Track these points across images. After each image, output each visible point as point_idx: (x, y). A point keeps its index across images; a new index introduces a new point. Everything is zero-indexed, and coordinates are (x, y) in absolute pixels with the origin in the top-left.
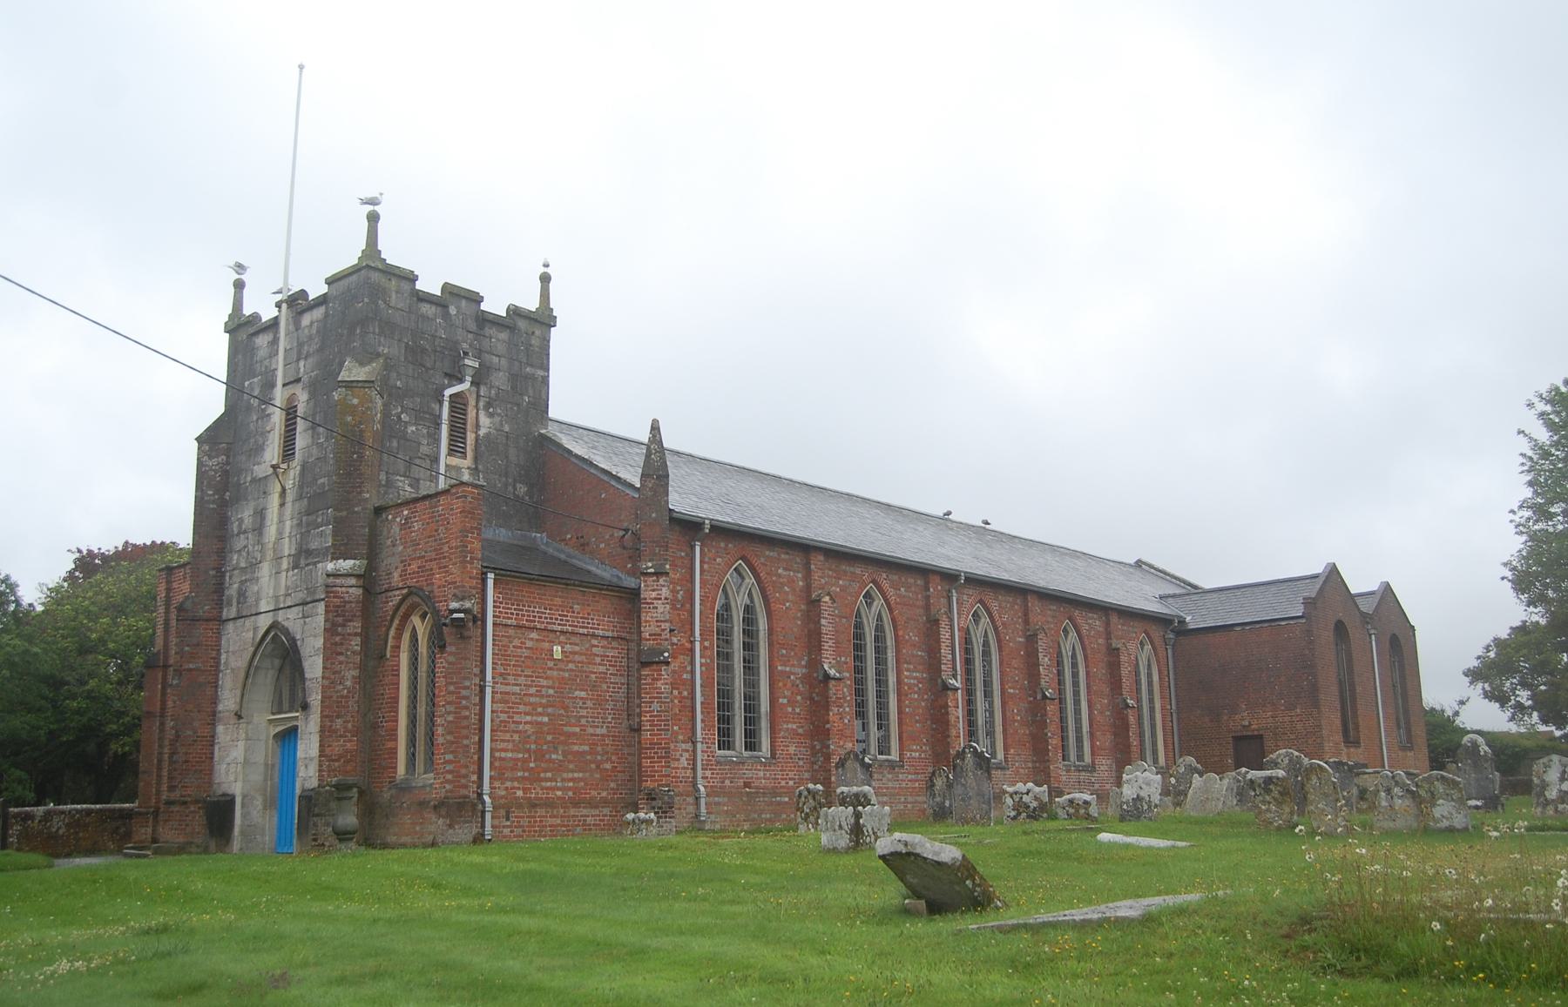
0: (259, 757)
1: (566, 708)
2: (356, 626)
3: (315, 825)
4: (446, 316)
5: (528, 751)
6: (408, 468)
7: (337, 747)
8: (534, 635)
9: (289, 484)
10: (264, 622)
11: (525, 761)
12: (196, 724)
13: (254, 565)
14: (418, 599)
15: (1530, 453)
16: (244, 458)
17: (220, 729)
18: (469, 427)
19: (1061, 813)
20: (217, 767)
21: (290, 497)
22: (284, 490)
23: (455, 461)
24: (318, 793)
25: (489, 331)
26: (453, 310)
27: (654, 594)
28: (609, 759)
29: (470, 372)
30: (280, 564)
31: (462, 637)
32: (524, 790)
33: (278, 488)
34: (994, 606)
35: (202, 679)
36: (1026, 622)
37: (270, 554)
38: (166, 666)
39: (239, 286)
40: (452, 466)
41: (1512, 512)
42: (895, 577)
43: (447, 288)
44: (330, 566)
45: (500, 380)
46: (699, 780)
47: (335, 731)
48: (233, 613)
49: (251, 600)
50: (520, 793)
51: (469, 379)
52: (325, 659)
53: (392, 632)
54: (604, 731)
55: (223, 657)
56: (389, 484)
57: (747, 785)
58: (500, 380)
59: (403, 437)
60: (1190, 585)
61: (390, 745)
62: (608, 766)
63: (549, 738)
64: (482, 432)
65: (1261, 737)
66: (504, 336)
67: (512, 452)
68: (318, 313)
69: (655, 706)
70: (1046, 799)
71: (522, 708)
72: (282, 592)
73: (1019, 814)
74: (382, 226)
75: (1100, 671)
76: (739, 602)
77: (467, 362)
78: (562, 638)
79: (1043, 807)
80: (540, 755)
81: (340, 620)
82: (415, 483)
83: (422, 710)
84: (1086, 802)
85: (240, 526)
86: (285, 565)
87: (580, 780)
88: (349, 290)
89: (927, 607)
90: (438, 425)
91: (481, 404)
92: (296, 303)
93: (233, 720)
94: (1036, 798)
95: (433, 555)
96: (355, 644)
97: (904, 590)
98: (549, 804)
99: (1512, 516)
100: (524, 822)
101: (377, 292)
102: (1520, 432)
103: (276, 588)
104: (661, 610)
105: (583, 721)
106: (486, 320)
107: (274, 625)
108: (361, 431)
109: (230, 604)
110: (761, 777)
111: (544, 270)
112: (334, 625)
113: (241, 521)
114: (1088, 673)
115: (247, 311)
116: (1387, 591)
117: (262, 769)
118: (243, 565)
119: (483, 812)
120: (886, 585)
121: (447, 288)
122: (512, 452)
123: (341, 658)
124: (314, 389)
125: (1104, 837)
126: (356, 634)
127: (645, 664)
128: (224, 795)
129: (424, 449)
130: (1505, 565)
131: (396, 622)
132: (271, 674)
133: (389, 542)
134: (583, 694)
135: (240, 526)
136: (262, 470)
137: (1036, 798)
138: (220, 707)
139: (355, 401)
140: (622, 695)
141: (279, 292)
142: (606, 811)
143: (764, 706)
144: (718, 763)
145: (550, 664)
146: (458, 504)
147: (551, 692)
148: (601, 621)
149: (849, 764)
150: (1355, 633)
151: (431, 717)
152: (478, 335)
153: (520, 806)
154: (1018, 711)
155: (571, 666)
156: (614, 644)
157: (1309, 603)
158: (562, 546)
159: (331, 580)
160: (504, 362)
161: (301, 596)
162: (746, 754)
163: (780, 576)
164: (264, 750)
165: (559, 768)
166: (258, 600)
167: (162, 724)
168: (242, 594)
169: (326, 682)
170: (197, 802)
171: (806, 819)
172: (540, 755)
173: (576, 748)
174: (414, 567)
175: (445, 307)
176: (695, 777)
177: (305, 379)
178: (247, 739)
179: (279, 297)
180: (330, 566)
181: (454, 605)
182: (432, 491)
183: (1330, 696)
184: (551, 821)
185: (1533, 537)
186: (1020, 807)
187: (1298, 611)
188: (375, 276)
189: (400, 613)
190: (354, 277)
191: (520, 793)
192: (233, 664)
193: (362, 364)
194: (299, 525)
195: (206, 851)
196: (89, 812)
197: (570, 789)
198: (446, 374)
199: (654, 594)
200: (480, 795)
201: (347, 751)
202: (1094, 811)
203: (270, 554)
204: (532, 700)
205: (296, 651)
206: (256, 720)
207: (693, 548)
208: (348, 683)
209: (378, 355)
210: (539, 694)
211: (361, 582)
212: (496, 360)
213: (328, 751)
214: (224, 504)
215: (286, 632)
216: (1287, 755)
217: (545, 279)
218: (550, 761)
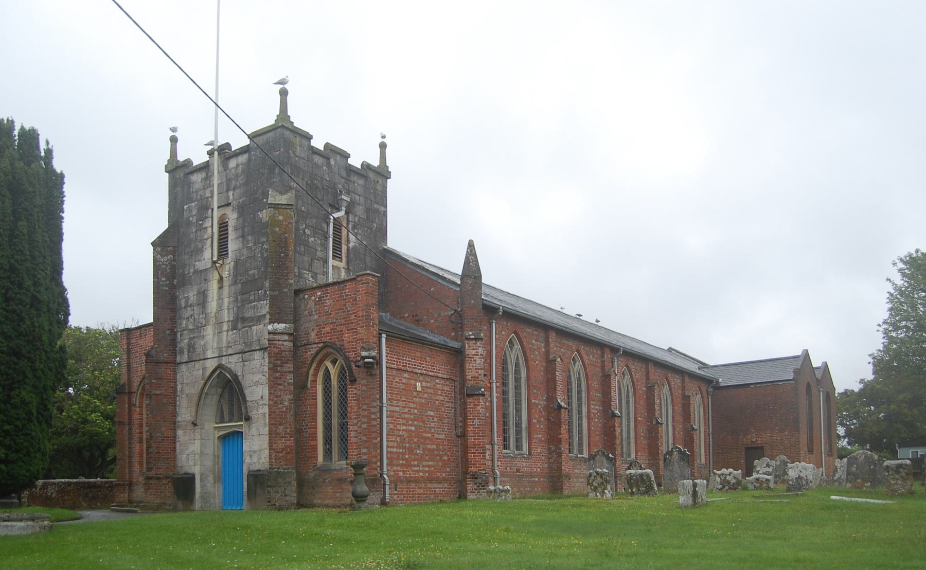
0: (210, 451)
1: (423, 422)
2: (289, 367)
3: (269, 492)
4: (329, 165)
5: (405, 448)
6: (311, 265)
7: (280, 444)
8: (406, 375)
9: (225, 274)
10: (211, 365)
11: (404, 454)
12: (163, 429)
13: (199, 328)
14: (330, 350)
15: (892, 291)
16: (187, 257)
17: (180, 432)
18: (343, 241)
19: (750, 486)
20: (179, 456)
21: (226, 283)
22: (221, 279)
23: (337, 263)
24: (270, 473)
25: (354, 178)
26: (332, 162)
27: (474, 352)
28: (446, 454)
29: (345, 204)
30: (221, 328)
31: (371, 375)
32: (404, 472)
33: (216, 276)
34: (633, 368)
35: (165, 401)
36: (648, 379)
37: (212, 320)
38: (130, 393)
39: (174, 140)
40: (336, 269)
41: (879, 325)
42: (587, 349)
43: (327, 146)
44: (270, 327)
45: (360, 210)
46: (496, 468)
47: (279, 434)
48: (185, 358)
49: (199, 350)
50: (401, 474)
51: (344, 208)
52: (270, 388)
53: (311, 371)
54: (442, 436)
55: (179, 387)
56: (300, 275)
57: (518, 471)
58: (360, 210)
59: (307, 245)
60: (701, 362)
61: (312, 443)
62: (446, 458)
63: (415, 440)
64: (351, 245)
65: (762, 448)
66: (361, 182)
67: (368, 259)
68: (243, 158)
69: (476, 422)
70: (740, 478)
71: (401, 421)
72: (224, 344)
73: (724, 487)
74: (289, 98)
75: (679, 409)
76: (512, 358)
77: (344, 197)
78: (421, 378)
79: (739, 483)
80: (411, 451)
81: (279, 362)
82: (315, 276)
83: (335, 421)
84: (767, 480)
85: (187, 302)
86: (225, 327)
87: (432, 466)
88: (268, 143)
89: (603, 367)
90: (327, 238)
91: (350, 226)
92: (224, 152)
93: (190, 427)
94: (735, 478)
95: (343, 321)
96: (290, 378)
97: (592, 356)
98: (416, 481)
99: (878, 328)
100: (405, 491)
101: (289, 145)
102: (888, 280)
103: (220, 341)
104: (478, 362)
105: (433, 430)
106: (351, 170)
107: (220, 366)
108: (286, 238)
109: (182, 352)
110: (524, 465)
111: (382, 140)
112: (275, 366)
113: (187, 299)
114: (673, 410)
115: (181, 158)
116: (825, 366)
117: (211, 458)
118: (191, 327)
119: (385, 485)
120: (583, 353)
121: (327, 146)
122: (368, 259)
123: (281, 387)
124: (242, 210)
125: (833, 497)
126: (290, 372)
127: (469, 396)
128: (186, 474)
129: (319, 254)
130: (870, 355)
131: (314, 365)
132: (215, 398)
133: (306, 313)
134: (432, 413)
135: (187, 302)
136: (200, 265)
137: (735, 478)
138: (179, 419)
139: (281, 218)
140: (451, 415)
141: (211, 144)
142: (446, 485)
143: (524, 424)
144: (504, 457)
145: (415, 394)
146: (362, 288)
147: (416, 411)
148: (440, 368)
149: (598, 458)
150: (814, 390)
151: (343, 427)
152: (348, 180)
153: (402, 482)
154: (642, 430)
155: (426, 396)
156: (448, 383)
157: (796, 372)
158: (402, 321)
159: (271, 336)
160: (362, 200)
161: (240, 348)
162: (516, 452)
163: (533, 345)
164: (212, 446)
165: (421, 459)
166: (205, 350)
167: (130, 429)
168: (191, 347)
169: (272, 403)
170: (167, 478)
171: (595, 489)
172: (411, 451)
173: (429, 446)
174: (328, 329)
175: (328, 159)
176: (493, 465)
177: (235, 203)
178: (202, 439)
179: (210, 147)
180: (270, 327)
181: (364, 354)
182: (324, 282)
183: (803, 427)
184: (419, 491)
185: (891, 340)
186: (725, 483)
187: (790, 376)
188: (287, 133)
189: (318, 358)
190: (271, 134)
191: (401, 474)
192: (187, 391)
193: (281, 193)
194: (236, 300)
195: (175, 509)
196: (70, 484)
197: (427, 471)
198: (330, 205)
199: (474, 352)
200: (382, 475)
201: (287, 446)
202: (772, 485)
203: (212, 320)
204: (406, 416)
205: (239, 383)
206: (206, 427)
207: (491, 324)
208: (286, 403)
209: (291, 188)
210: (409, 413)
211: (291, 338)
212: (357, 197)
213: (274, 446)
214: (173, 287)
215: (230, 371)
216: (863, 453)
217: (383, 146)
218: (417, 454)
